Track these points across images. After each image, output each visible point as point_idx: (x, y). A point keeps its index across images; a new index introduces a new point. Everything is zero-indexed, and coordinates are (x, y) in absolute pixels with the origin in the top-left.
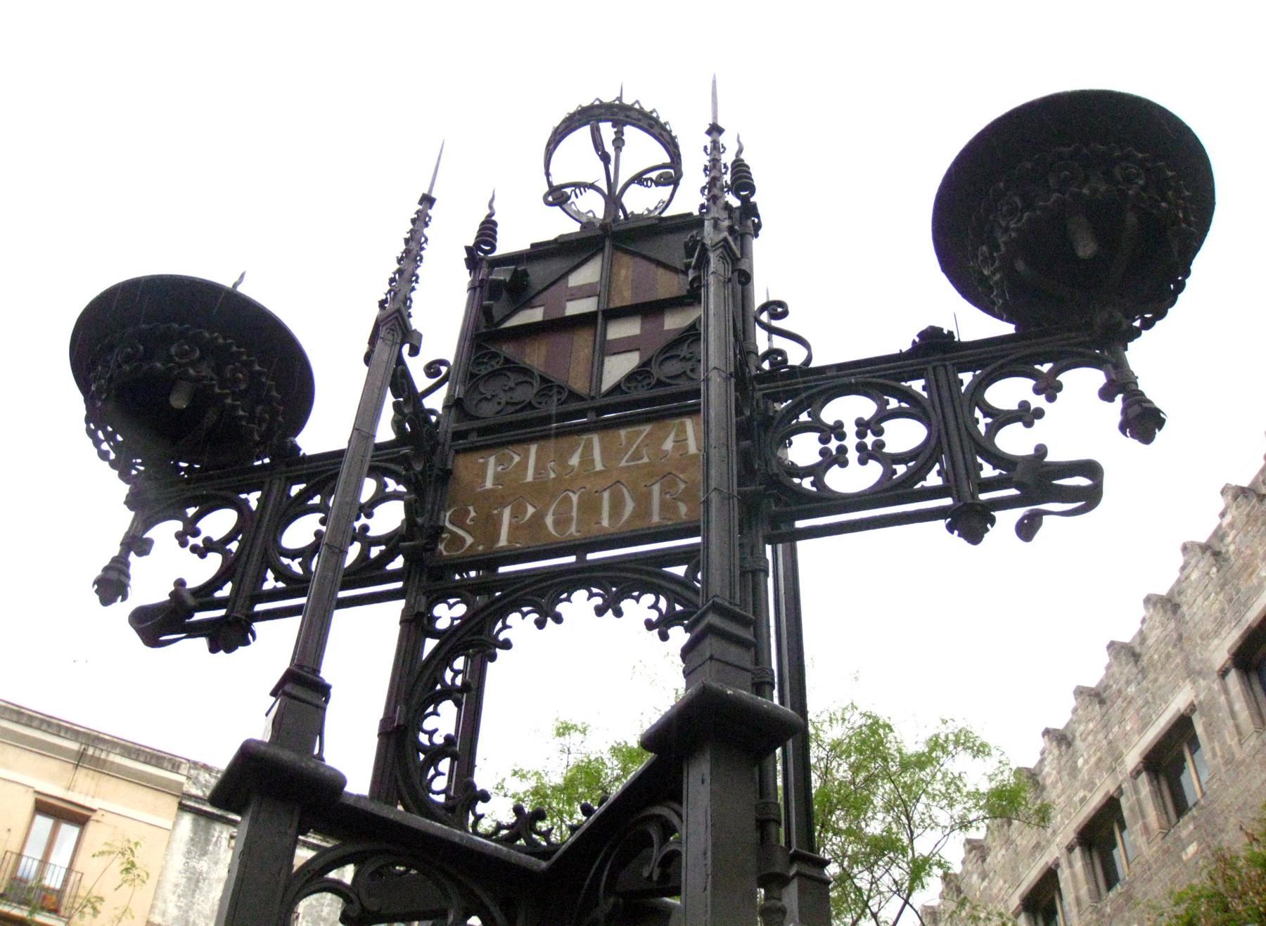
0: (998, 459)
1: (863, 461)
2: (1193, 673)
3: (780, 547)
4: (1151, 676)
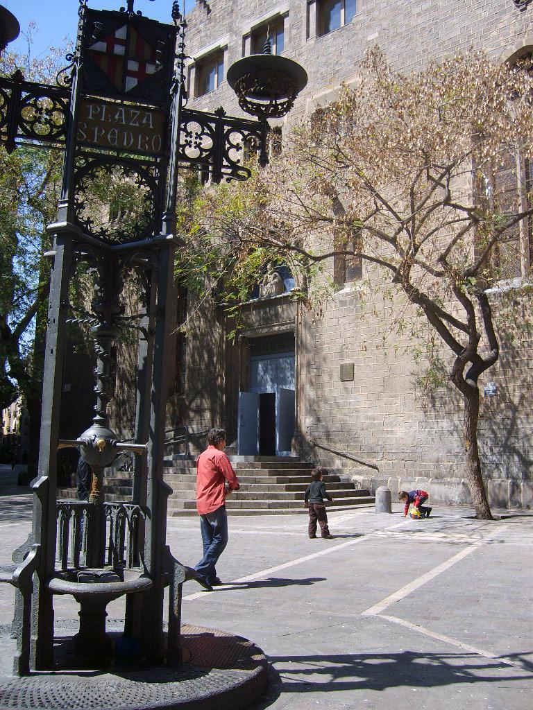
0: (228, 160)
1: (191, 132)
2: (231, 30)
3: (327, 508)
4: (212, 24)
